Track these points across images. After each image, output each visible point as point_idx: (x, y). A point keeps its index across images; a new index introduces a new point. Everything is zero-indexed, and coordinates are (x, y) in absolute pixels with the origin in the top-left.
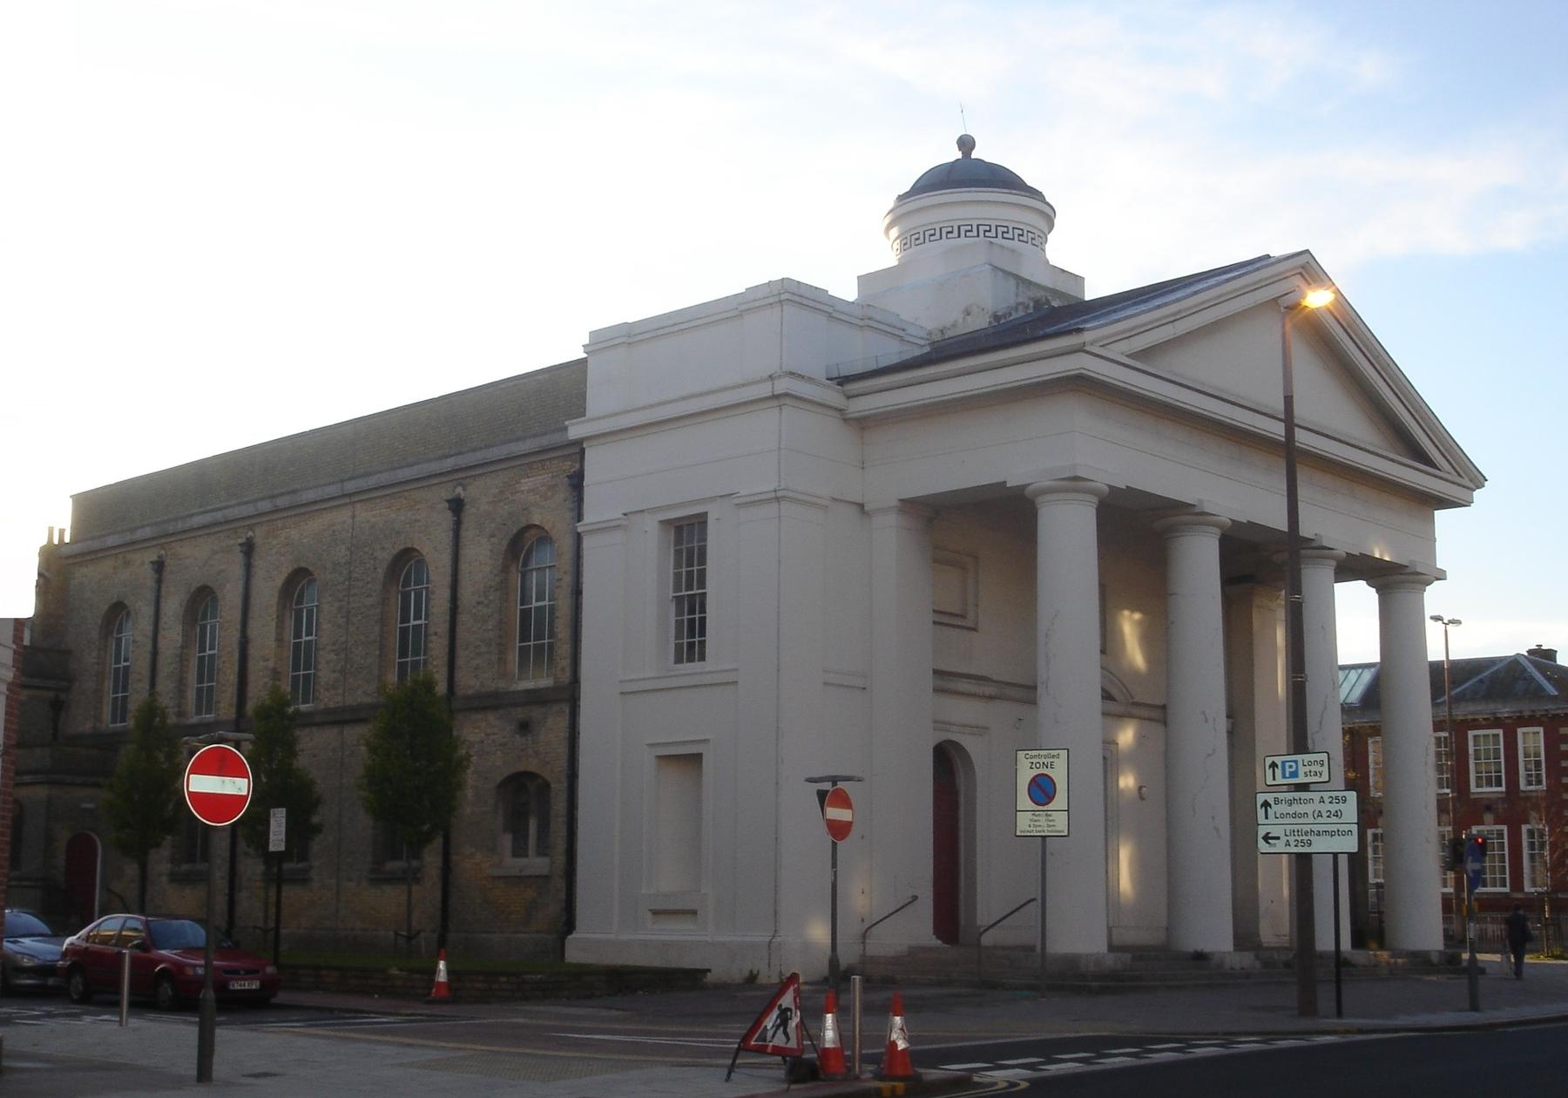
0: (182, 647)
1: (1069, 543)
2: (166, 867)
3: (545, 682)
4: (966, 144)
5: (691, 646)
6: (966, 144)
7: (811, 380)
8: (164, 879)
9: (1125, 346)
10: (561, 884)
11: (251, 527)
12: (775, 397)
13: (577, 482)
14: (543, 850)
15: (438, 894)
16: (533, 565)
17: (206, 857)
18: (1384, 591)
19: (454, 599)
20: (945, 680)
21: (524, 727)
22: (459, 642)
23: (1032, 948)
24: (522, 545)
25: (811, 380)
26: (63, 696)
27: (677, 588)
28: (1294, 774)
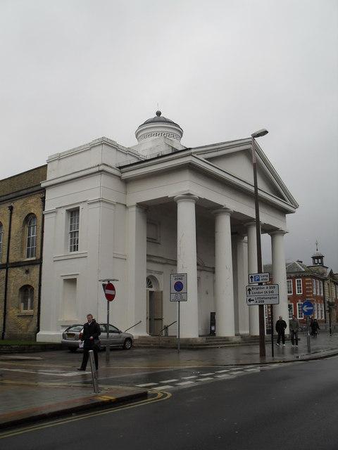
1: (186, 218)
3: (34, 258)
4: (159, 114)
6: (159, 114)
7: (111, 167)
9: (203, 156)
10: (36, 318)
11: (11, 202)
13: (43, 200)
14: (32, 308)
18: (273, 236)
19: (9, 235)
20: (150, 259)
21: (27, 272)
22: (10, 248)
23: (176, 336)
24: (29, 219)
25: (111, 167)
27: (71, 230)
28: (258, 280)
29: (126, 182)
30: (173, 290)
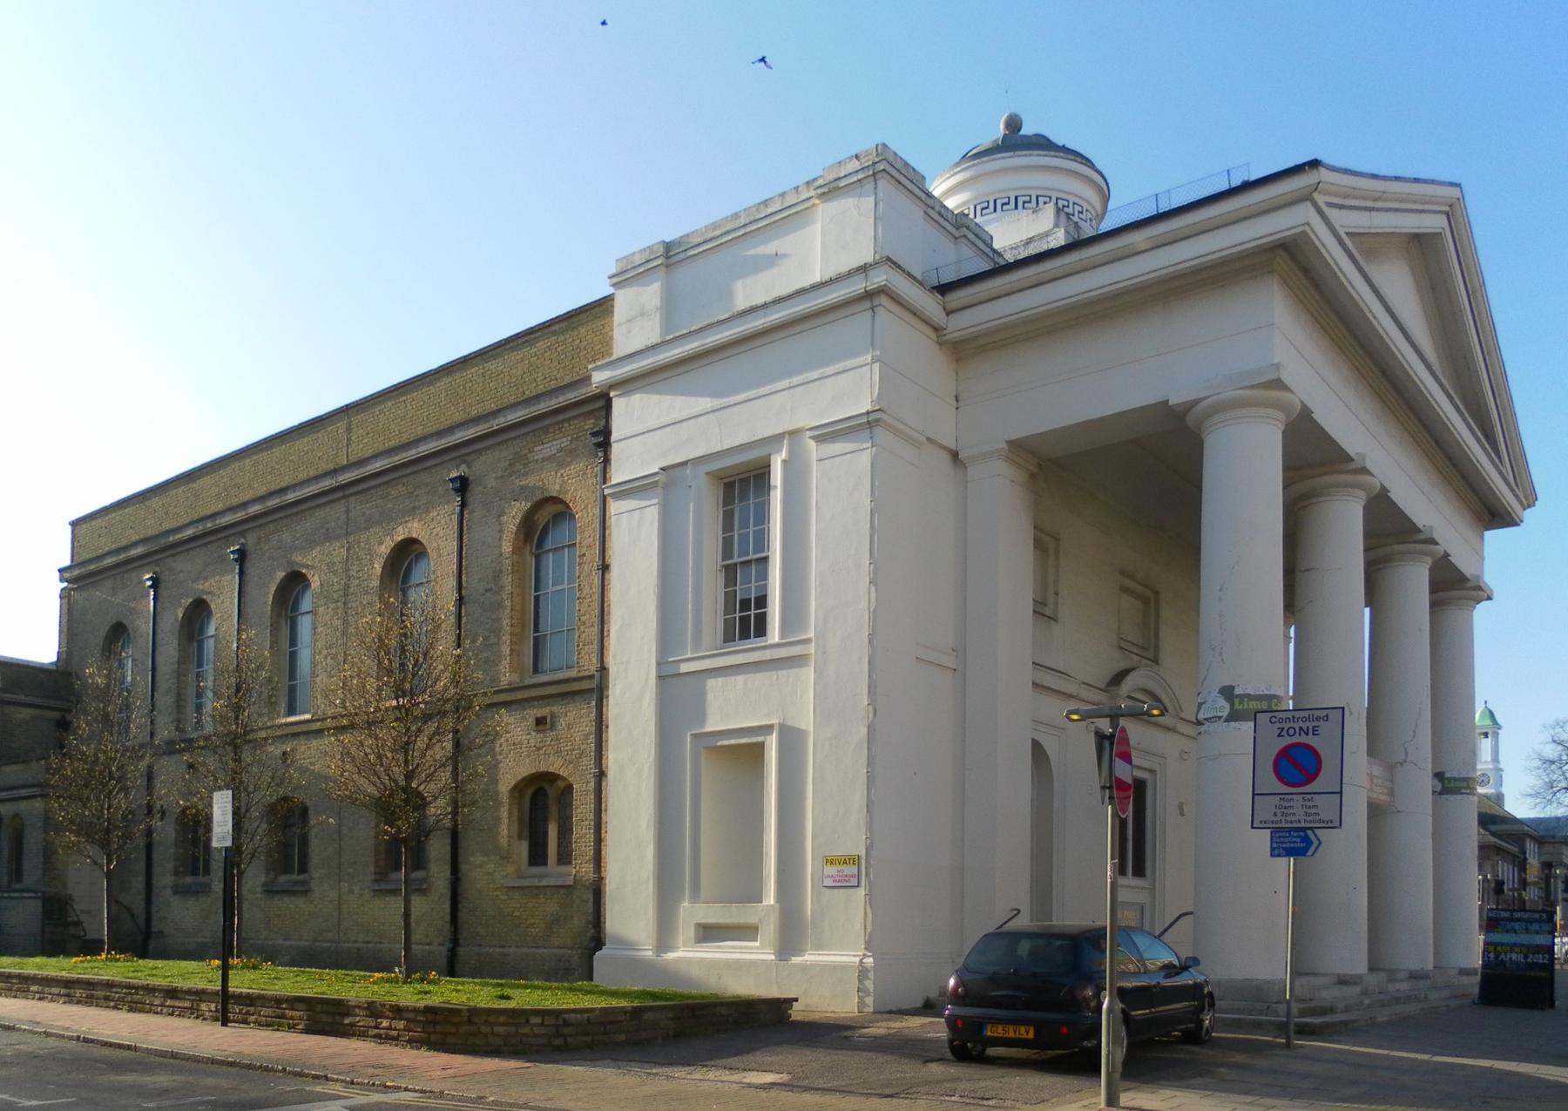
0: (179, 663)
2: (169, 879)
5: (745, 621)
8: (169, 891)
11: (242, 534)
12: (869, 295)
13: (603, 441)
15: (447, 907)
16: (549, 544)
17: (207, 871)
26: (69, 717)
29: (962, 350)
30: (1271, 783)
